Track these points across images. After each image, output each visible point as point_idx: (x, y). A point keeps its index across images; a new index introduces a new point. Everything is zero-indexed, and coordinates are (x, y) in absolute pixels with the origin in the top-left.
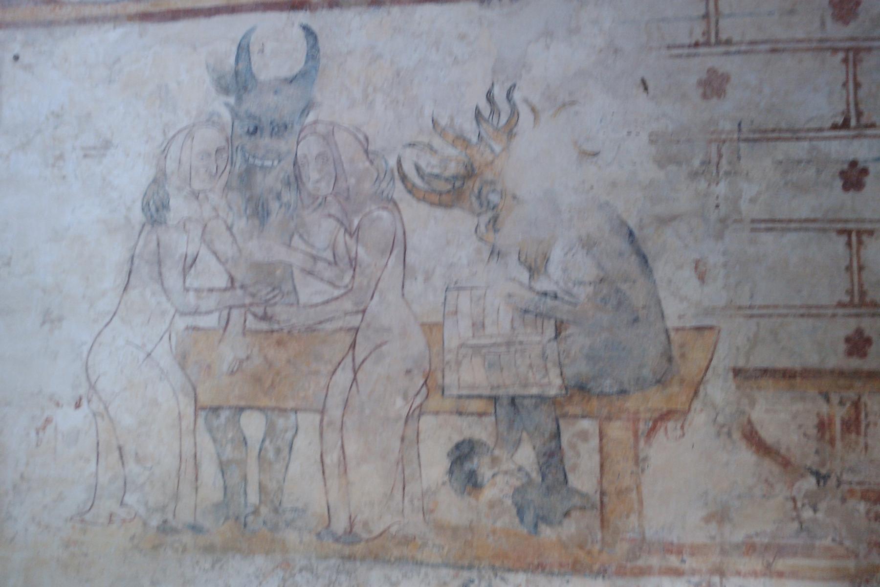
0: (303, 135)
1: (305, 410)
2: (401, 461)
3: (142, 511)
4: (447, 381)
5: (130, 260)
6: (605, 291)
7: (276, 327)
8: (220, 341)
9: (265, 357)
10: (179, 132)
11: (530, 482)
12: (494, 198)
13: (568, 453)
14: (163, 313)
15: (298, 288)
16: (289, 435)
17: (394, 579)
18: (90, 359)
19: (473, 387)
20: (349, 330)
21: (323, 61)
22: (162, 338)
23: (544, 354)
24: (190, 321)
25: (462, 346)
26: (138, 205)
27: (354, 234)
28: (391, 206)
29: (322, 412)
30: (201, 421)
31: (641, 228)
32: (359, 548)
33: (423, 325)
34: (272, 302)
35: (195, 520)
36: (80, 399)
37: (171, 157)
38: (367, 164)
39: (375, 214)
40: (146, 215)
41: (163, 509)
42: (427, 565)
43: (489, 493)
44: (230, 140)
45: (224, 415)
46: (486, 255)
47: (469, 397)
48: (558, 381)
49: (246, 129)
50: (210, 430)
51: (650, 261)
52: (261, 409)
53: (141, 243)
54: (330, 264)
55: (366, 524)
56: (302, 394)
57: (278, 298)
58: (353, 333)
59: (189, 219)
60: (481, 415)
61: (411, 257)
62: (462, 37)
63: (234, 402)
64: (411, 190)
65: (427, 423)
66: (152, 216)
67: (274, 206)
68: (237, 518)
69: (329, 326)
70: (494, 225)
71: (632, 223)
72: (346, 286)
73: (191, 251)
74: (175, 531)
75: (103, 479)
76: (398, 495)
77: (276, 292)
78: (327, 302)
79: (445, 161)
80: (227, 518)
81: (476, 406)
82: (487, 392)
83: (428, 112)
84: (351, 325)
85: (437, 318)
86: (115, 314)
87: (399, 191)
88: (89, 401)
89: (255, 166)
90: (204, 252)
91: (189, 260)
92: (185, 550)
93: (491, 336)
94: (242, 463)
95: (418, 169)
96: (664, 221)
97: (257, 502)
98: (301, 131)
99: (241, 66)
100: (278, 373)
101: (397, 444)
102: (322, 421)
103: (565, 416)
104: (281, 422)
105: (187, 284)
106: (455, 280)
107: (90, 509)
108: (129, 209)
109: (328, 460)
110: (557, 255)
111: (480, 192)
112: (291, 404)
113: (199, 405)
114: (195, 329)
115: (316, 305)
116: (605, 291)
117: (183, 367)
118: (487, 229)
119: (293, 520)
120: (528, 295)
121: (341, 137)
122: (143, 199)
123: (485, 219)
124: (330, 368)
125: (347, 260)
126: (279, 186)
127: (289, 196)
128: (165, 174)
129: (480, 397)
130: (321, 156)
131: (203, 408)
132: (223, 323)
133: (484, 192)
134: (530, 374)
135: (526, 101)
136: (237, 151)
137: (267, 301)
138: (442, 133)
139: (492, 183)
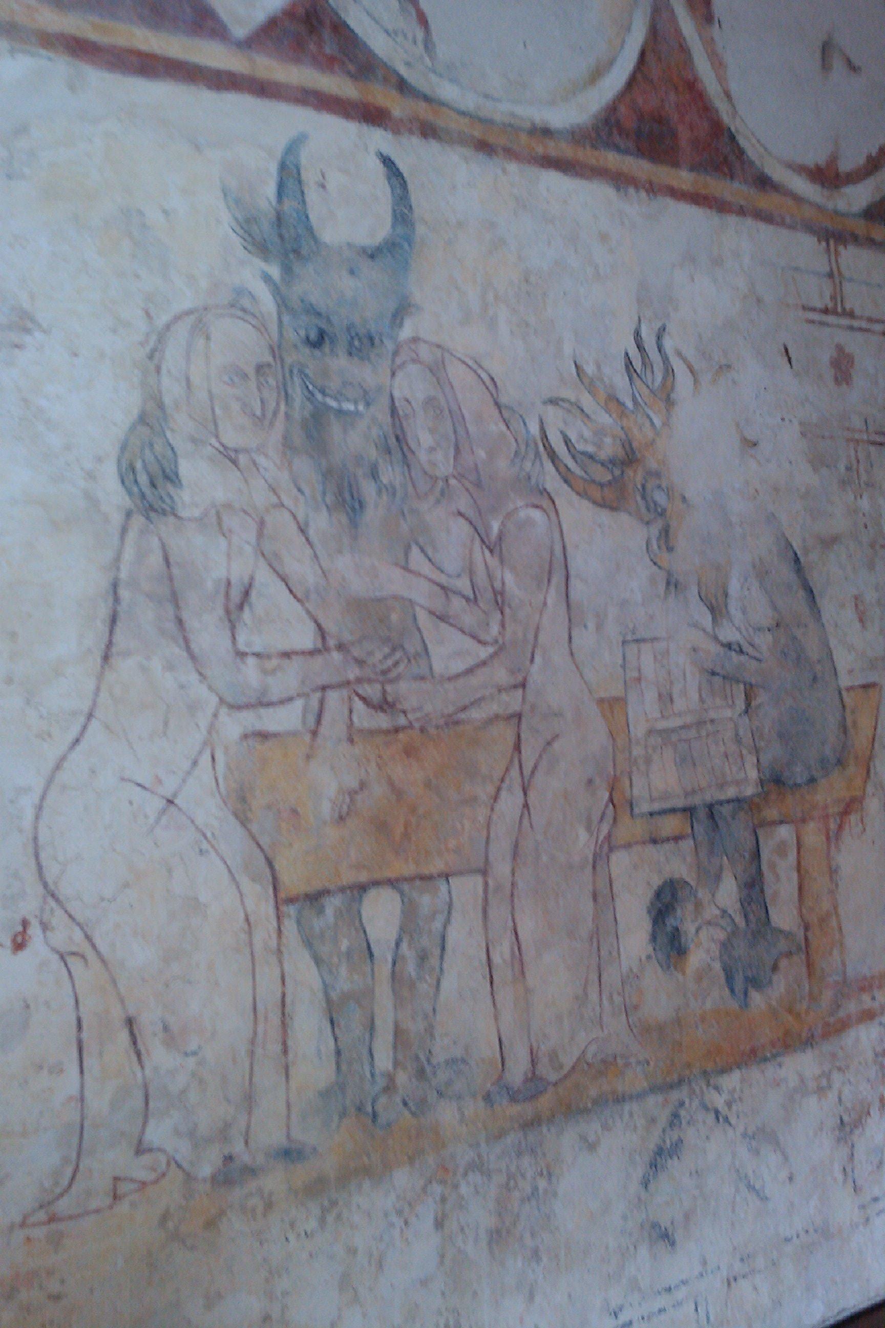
0: (398, 361)
1: (460, 873)
2: (596, 936)
3: (183, 1150)
4: (636, 792)
5: (111, 592)
6: (783, 641)
7: (402, 721)
8: (308, 757)
9: (391, 783)
10: (177, 318)
11: (735, 932)
12: (660, 498)
13: (768, 876)
14: (193, 708)
15: (430, 646)
16: (437, 925)
17: (592, 1138)
18: (42, 825)
19: (665, 796)
20: (509, 718)
21: (421, 229)
22: (195, 763)
23: (737, 735)
24: (249, 720)
25: (650, 732)
26: (109, 472)
27: (494, 547)
28: (546, 503)
29: (484, 872)
30: (290, 927)
31: (806, 551)
32: (545, 1102)
33: (601, 701)
34: (393, 674)
35: (288, 1137)
36: (25, 923)
37: (169, 372)
38: (503, 427)
39: (522, 514)
40: (130, 493)
41: (223, 1133)
42: (631, 1097)
43: (696, 959)
44: (276, 351)
45: (332, 904)
46: (662, 587)
47: (663, 812)
48: (753, 774)
49: (302, 333)
50: (308, 943)
51: (817, 597)
52: (391, 883)
53: (129, 554)
54: (467, 599)
55: (553, 1056)
56: (452, 843)
57: (401, 667)
58: (515, 720)
59: (228, 506)
60: (677, 839)
61: (578, 589)
62: (604, 237)
63: (349, 877)
64: (567, 478)
65: (620, 862)
66: (143, 496)
67: (368, 489)
68: (360, 1109)
69: (476, 714)
70: (667, 542)
71: (796, 544)
72: (496, 641)
73: (239, 571)
74: (250, 1171)
75: (98, 1104)
76: (594, 996)
77: (398, 655)
78: (470, 671)
79: (600, 432)
80: (343, 1114)
81: (670, 825)
82: (680, 803)
83: (568, 349)
84: (510, 711)
85: (616, 690)
86: (90, 716)
87: (551, 480)
88: (45, 927)
89: (329, 408)
90: (264, 577)
91: (236, 594)
92: (269, 1206)
93: (680, 715)
94: (363, 998)
95: (567, 441)
96: (829, 542)
97: (390, 1067)
98: (396, 353)
99: (289, 205)
100: (413, 810)
101: (588, 906)
102: (486, 884)
103: (763, 824)
104: (425, 901)
105: (241, 639)
106: (631, 626)
107: (70, 1185)
108: (91, 476)
109: (497, 959)
110: (734, 587)
111: (643, 486)
112: (437, 865)
113: (282, 895)
114: (264, 736)
115: (457, 676)
116: (783, 641)
117: (244, 822)
118: (659, 547)
119: (449, 1083)
120: (714, 648)
121: (457, 373)
122: (119, 461)
123: (655, 530)
124: (491, 789)
125: (489, 595)
126: (373, 454)
127: (390, 474)
128: (161, 406)
129: (673, 811)
130: (430, 402)
131: (291, 900)
132: (311, 720)
133: (649, 486)
134: (727, 768)
135: (679, 354)
136: (291, 377)
137: (384, 672)
138: (592, 389)
139: (658, 475)
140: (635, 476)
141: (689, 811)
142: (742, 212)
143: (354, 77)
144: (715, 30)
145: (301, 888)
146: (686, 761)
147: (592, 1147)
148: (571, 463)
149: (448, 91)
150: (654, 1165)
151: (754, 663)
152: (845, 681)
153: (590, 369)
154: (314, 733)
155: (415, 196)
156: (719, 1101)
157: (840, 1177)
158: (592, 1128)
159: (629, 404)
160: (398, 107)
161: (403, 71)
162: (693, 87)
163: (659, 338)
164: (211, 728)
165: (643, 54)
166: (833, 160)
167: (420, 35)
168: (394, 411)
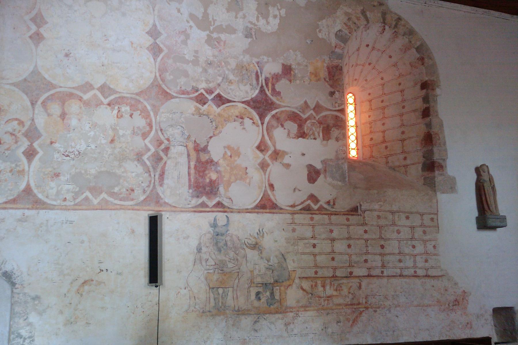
3: (199, 309)
9: (222, 278)
12: (261, 248)
19: (259, 282)
24: (207, 271)
27: (237, 254)
30: (210, 291)
32: (240, 312)
33: (250, 271)
41: (203, 308)
43: (262, 301)
45: (215, 289)
46: (260, 258)
48: (273, 280)
60: (260, 287)
65: (251, 289)
67: (222, 249)
73: (207, 258)
74: (206, 312)
83: (249, 232)
87: (245, 247)
88: (187, 288)
90: (210, 258)
95: (248, 243)
96: (288, 253)
109: (234, 297)
112: (227, 286)
117: (206, 281)
121: (234, 237)
124: (234, 279)
126: (223, 246)
127: (225, 247)
130: (230, 240)
135: (265, 231)
138: (252, 236)
139: (261, 246)
140: (257, 246)
141: (263, 284)
142: (277, 213)
143: (223, 208)
144: (274, 192)
145: (212, 287)
146: (262, 278)
147: (246, 319)
148: (248, 245)
149: (234, 207)
150: (255, 322)
151: (274, 267)
152: (290, 270)
153: (252, 234)
154: (214, 273)
155: (230, 219)
156: (265, 317)
157: (285, 330)
158: (246, 317)
159: (257, 238)
160: (228, 210)
161: (229, 206)
162: (270, 200)
163: (262, 230)
164: (204, 272)
165: (262, 197)
166: (294, 204)
167: (231, 202)
168: (226, 241)
